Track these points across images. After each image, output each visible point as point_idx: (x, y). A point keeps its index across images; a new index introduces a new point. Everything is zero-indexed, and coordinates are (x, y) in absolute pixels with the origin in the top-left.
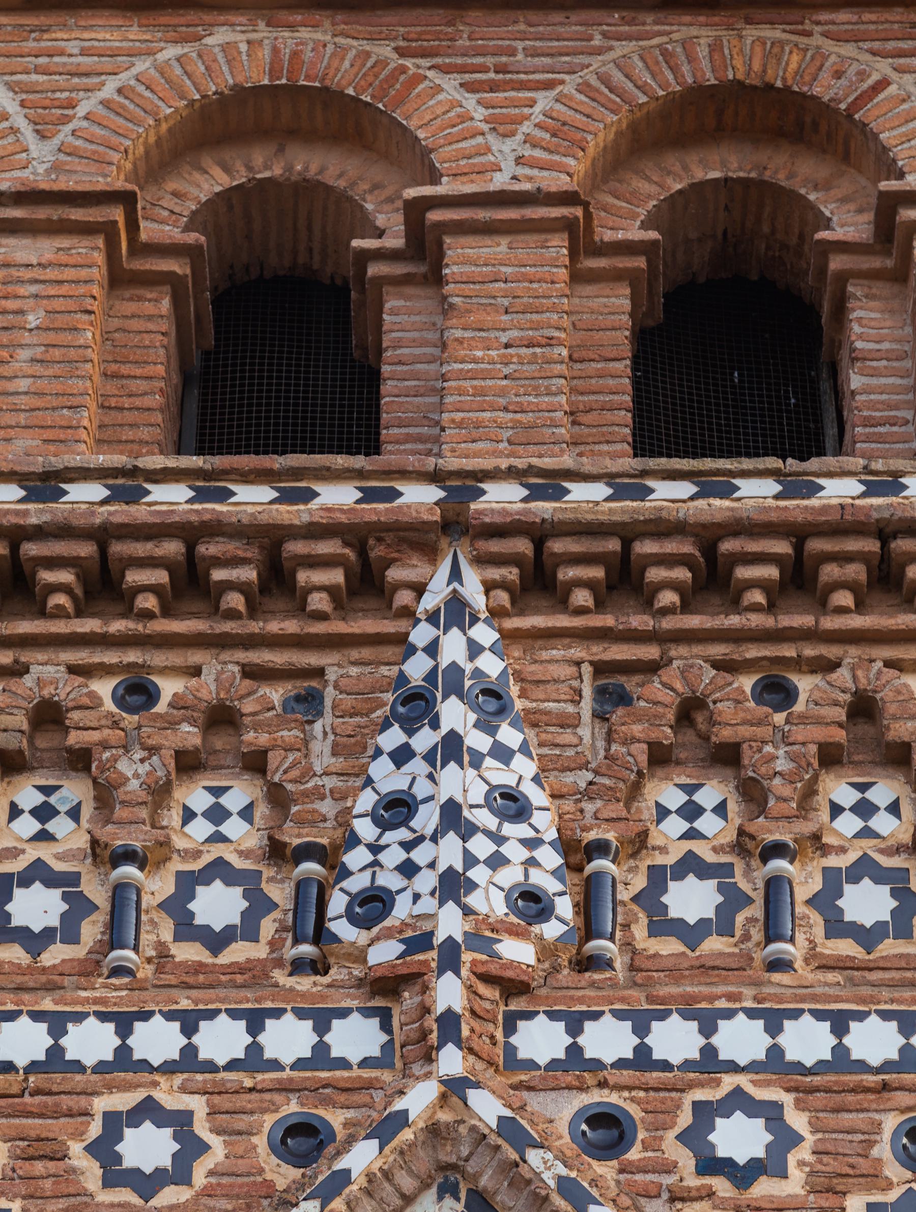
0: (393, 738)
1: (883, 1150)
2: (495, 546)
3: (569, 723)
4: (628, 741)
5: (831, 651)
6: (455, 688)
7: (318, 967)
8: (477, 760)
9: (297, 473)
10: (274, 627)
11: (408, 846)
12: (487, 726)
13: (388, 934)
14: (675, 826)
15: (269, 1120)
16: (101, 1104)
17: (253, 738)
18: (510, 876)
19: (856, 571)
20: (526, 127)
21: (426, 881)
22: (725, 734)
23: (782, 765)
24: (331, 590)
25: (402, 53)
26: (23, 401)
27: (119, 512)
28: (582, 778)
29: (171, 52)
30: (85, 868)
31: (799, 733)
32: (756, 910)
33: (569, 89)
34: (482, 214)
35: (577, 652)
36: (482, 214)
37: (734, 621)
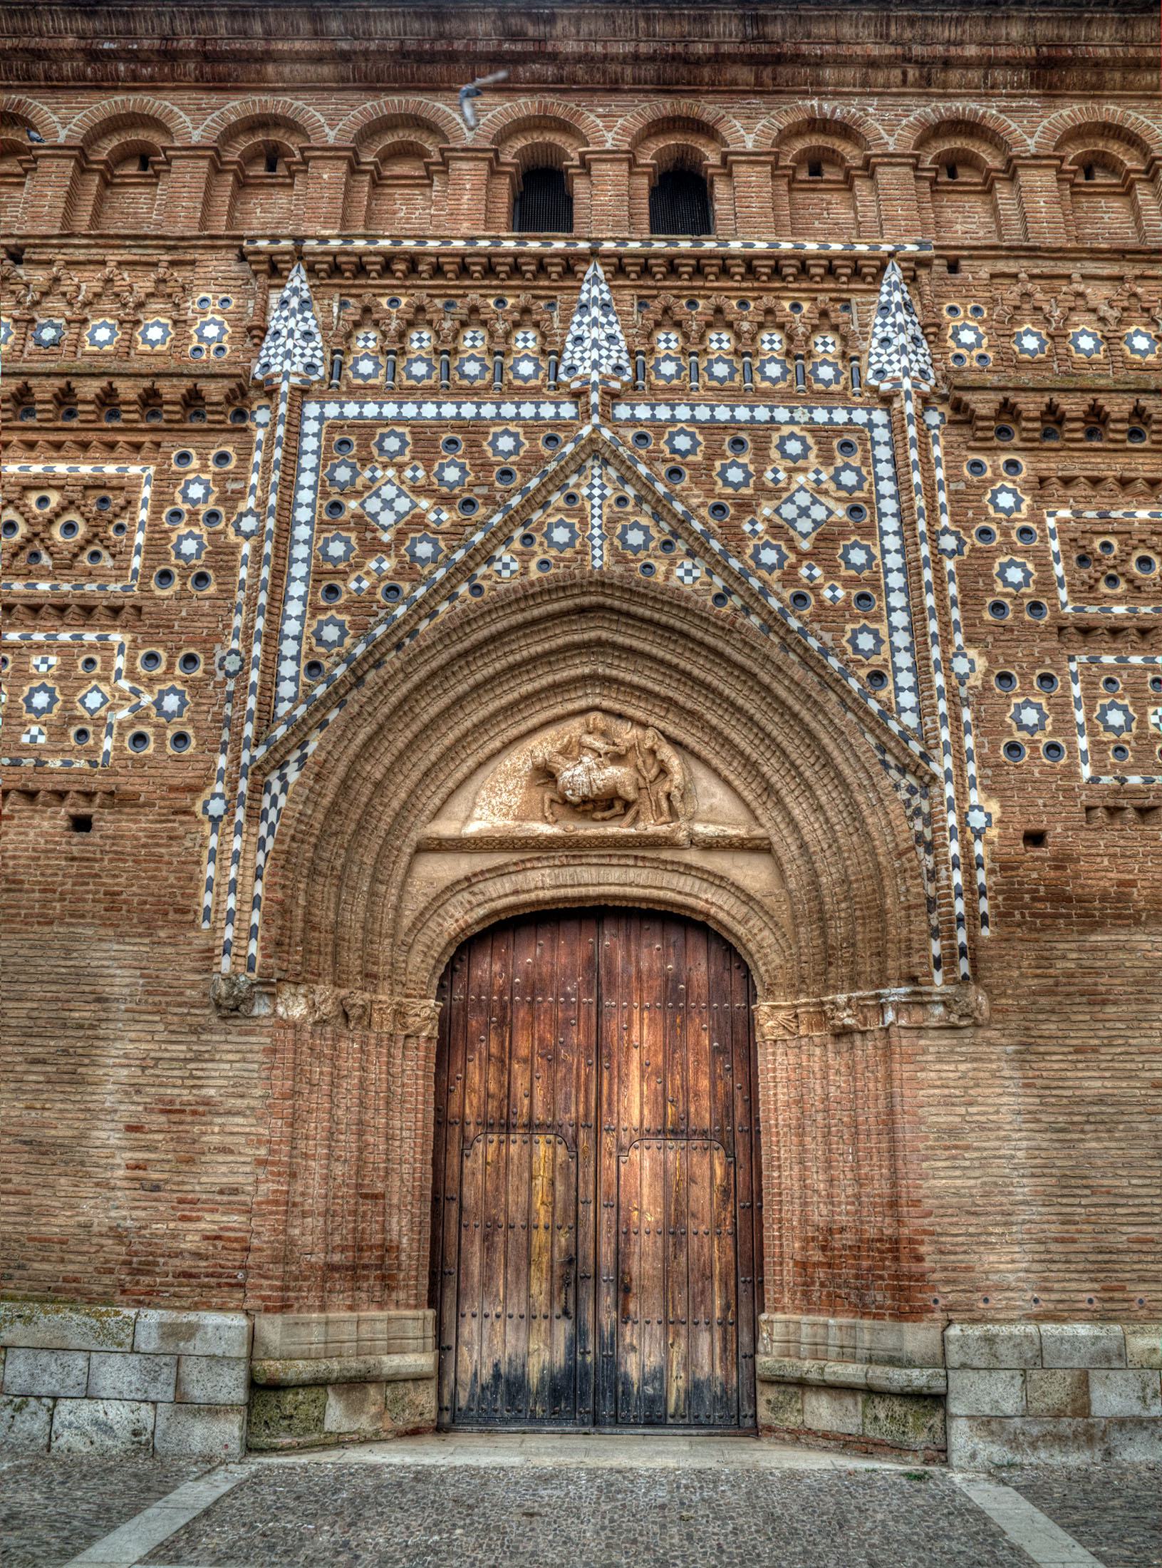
1: (726, 447)
12: (606, 315)
16: (492, 430)
17: (536, 317)
18: (613, 362)
19: (715, 269)
21: (587, 363)
27: (470, 250)
28: (634, 331)
30: (433, 357)
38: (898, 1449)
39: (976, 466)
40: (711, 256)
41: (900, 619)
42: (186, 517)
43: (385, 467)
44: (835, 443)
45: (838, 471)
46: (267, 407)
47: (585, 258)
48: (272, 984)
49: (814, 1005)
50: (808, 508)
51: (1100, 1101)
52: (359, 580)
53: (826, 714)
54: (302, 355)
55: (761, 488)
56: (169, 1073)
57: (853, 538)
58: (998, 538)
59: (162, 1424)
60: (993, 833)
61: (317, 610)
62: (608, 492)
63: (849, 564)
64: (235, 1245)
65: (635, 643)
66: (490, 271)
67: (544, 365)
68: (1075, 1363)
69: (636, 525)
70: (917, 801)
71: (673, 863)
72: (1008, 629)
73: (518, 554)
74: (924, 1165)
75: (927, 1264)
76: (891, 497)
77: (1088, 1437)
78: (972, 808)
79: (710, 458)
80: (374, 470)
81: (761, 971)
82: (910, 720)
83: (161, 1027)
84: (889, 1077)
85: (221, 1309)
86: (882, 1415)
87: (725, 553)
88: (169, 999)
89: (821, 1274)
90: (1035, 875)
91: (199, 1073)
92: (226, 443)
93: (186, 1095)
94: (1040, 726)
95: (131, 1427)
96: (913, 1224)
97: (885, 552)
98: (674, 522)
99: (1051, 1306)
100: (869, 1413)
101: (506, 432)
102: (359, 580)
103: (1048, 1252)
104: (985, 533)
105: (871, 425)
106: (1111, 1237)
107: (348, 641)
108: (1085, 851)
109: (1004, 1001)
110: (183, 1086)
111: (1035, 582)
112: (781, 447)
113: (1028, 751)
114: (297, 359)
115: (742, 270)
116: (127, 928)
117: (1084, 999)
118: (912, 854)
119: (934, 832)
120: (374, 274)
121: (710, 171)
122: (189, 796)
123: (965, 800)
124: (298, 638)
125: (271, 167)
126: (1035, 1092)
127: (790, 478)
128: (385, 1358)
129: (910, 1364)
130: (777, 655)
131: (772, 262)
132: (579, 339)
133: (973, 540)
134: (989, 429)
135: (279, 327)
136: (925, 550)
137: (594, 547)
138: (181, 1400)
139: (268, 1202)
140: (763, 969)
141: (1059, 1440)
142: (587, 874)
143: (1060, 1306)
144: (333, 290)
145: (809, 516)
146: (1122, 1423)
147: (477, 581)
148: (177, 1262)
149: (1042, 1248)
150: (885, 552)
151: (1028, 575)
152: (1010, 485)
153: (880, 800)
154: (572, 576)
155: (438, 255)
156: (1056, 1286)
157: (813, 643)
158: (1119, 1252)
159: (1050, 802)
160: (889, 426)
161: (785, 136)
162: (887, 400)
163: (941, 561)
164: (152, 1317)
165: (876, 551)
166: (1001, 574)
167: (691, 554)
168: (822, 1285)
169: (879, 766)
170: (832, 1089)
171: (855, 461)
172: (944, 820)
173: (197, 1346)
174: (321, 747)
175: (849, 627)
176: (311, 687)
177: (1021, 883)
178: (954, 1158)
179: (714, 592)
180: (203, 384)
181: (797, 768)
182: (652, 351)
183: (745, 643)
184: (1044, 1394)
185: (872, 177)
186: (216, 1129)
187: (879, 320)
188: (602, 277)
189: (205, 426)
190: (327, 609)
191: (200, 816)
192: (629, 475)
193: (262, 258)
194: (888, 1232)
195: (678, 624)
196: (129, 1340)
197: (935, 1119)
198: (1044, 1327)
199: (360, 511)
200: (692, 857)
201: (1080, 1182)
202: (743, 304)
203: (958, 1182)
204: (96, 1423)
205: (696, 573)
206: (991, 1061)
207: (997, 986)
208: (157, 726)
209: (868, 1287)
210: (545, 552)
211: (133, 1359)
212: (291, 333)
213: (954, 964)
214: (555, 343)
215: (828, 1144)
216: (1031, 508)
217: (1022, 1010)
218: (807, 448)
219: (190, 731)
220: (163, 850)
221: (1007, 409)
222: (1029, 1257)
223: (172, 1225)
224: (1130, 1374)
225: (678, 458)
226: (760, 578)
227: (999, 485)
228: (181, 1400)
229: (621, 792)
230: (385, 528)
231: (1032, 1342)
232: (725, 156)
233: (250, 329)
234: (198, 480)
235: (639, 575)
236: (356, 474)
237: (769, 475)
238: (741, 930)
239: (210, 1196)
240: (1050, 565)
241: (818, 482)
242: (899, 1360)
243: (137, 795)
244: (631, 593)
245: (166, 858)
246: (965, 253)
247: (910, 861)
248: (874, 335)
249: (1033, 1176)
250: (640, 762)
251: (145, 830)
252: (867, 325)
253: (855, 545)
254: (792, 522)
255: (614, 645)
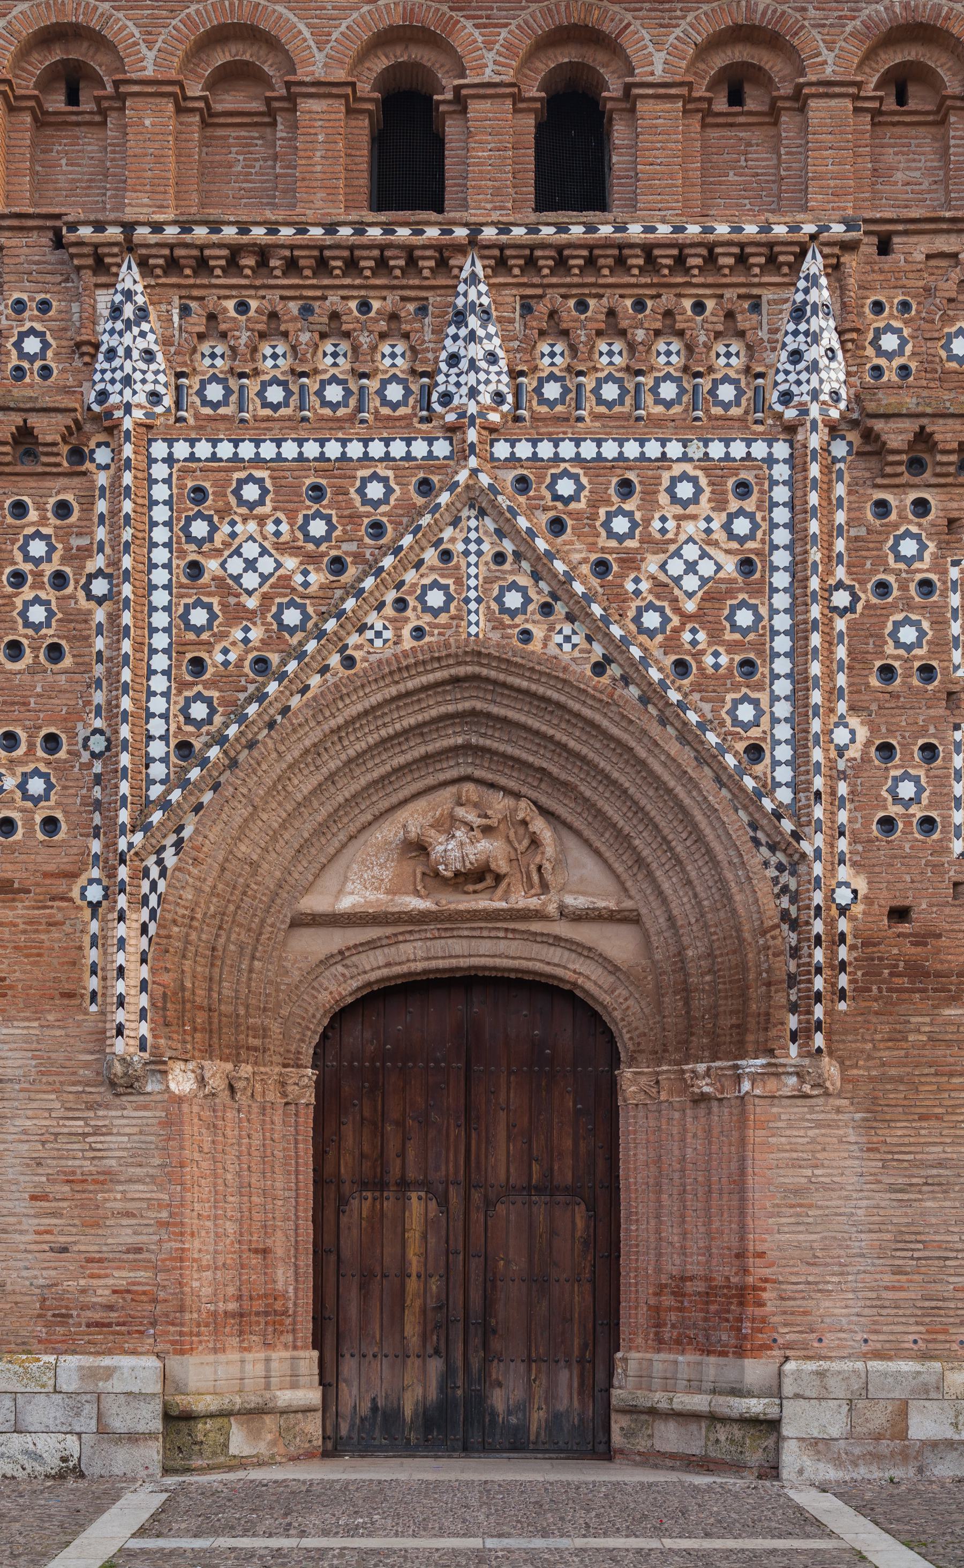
0: (452, 330)
2: (487, 252)
3: (511, 321)
4: (532, 328)
5: (601, 291)
6: (473, 311)
7: (428, 420)
8: (481, 339)
9: (418, 223)
10: (411, 282)
11: (458, 375)
12: (484, 326)
13: (452, 410)
14: (547, 361)
15: (414, 480)
17: (405, 327)
18: (492, 387)
20: (497, 46)
21: (464, 390)
22: (564, 326)
23: (583, 339)
24: (431, 268)
25: (451, 9)
26: (319, 176)
27: (329, 239)
29: (366, 8)
30: (290, 378)
31: (590, 325)
32: (573, 395)
33: (513, 27)
34: (482, 91)
35: (514, 292)
36: (482, 91)
37: (568, 280)
38: (737, 1467)
39: (882, 507)
40: (607, 244)
41: (783, 687)
42: (30, 579)
43: (245, 520)
44: (730, 483)
45: (731, 517)
46: (107, 445)
47: (460, 249)
48: (165, 1063)
49: (675, 1072)
50: (695, 563)
51: (940, 1165)
52: (225, 651)
53: (700, 791)
54: (144, 381)
55: (647, 539)
56: (69, 1146)
57: (741, 596)
58: (895, 593)
59: (87, 1451)
60: (858, 909)
61: (183, 685)
62: (485, 547)
63: (734, 628)
64: (143, 1298)
65: (511, 714)
66: (352, 265)
67: (414, 388)
68: (896, 1395)
69: (514, 586)
70: (785, 878)
71: (542, 934)
72: (894, 696)
73: (391, 620)
74: (771, 1221)
75: (769, 1308)
76: (785, 547)
77: (904, 1456)
78: (840, 884)
79: (594, 504)
80: (233, 523)
81: (625, 1041)
82: (784, 795)
83: (57, 1105)
84: (743, 1142)
85: (134, 1353)
86: (722, 1438)
87: (605, 620)
88: (62, 1079)
89: (673, 1317)
90: (895, 951)
91: (99, 1146)
92: (65, 489)
93: (88, 1166)
94: (915, 800)
95: (59, 1455)
96: (758, 1271)
97: (773, 612)
98: (554, 583)
99: (879, 1346)
100: (712, 1437)
101: (375, 477)
102: (225, 651)
103: (878, 1298)
104: (883, 588)
105: (770, 461)
106: (939, 1287)
107: (218, 719)
108: (948, 927)
109: (855, 1072)
110: (84, 1158)
111: (928, 643)
112: (671, 490)
113: (901, 826)
114: (138, 387)
115: (641, 262)
116: (14, 1012)
117: (932, 1070)
118: (777, 932)
119: (799, 909)
120: (218, 272)
121: (609, 105)
122: (64, 881)
123: (834, 876)
124: (165, 716)
125: (73, 98)
126: (878, 1156)
127: (679, 526)
128: (278, 1393)
129: (750, 1394)
130: (655, 730)
131: (675, 252)
132: (454, 359)
133: (867, 596)
134: (899, 463)
135: (113, 343)
136: (815, 611)
137: (469, 612)
138: (103, 1430)
139: (172, 1259)
140: (627, 1036)
141: (876, 1457)
142: (458, 946)
143: (887, 1346)
144: (171, 291)
145: (696, 573)
146: (934, 1445)
147: (349, 652)
148: (89, 1314)
149: (874, 1295)
150: (773, 612)
151: (922, 633)
152: (914, 529)
153: (749, 879)
154: (447, 645)
155: (292, 247)
156: (885, 1328)
157: (692, 717)
158: (944, 1300)
159: (918, 878)
160: (790, 461)
161: (705, 49)
162: (790, 429)
163: (831, 620)
164: (71, 1362)
165: (763, 611)
166: (894, 634)
167: (571, 618)
168: (673, 1326)
169: (750, 844)
170: (689, 1151)
171: (750, 505)
172: (810, 899)
173: (116, 1385)
174: (196, 831)
175: (729, 697)
176: (186, 770)
177: (881, 959)
178: (799, 1215)
179: (593, 660)
180: (35, 421)
181: (668, 843)
182: (535, 369)
183: (624, 717)
184: (867, 1420)
185: (802, 109)
186: (119, 1196)
187: (791, 327)
188: (481, 273)
189: (40, 469)
190: (194, 684)
191: (79, 902)
192: (506, 528)
193: (86, 250)
194: (734, 1280)
195: (555, 696)
196: (51, 1382)
197: (782, 1180)
198: (870, 1363)
199: (220, 573)
200: (562, 929)
201: (913, 1237)
202: (639, 305)
203: (801, 1237)
204: (26, 1452)
205: (575, 639)
206: (838, 1127)
207: (850, 1058)
208: (23, 810)
209: (714, 1329)
210: (419, 618)
211: (57, 1398)
212: (128, 352)
213: (810, 1038)
214: (425, 361)
215: (683, 1201)
216: (935, 557)
217: (871, 1079)
218: (699, 491)
219: (59, 815)
220: (43, 937)
221: (923, 438)
222: (862, 1303)
223: (82, 1282)
224: (946, 1403)
225: (559, 505)
226: (641, 645)
227: (902, 529)
228: (103, 1430)
229: (493, 866)
230: (249, 593)
231: (859, 1376)
232: (628, 87)
233: (78, 345)
234: (37, 535)
235: (515, 642)
236: (214, 529)
237: (657, 524)
238: (607, 999)
239: (118, 1256)
240: (947, 623)
241: (708, 531)
242: (740, 1390)
243: (12, 882)
244: (507, 664)
245: (47, 944)
246: (900, 227)
247: (774, 938)
248: (784, 345)
249: (870, 1231)
250: (512, 834)
251: (22, 916)
252: (777, 331)
253: (743, 604)
254: (677, 580)
255: (489, 715)
